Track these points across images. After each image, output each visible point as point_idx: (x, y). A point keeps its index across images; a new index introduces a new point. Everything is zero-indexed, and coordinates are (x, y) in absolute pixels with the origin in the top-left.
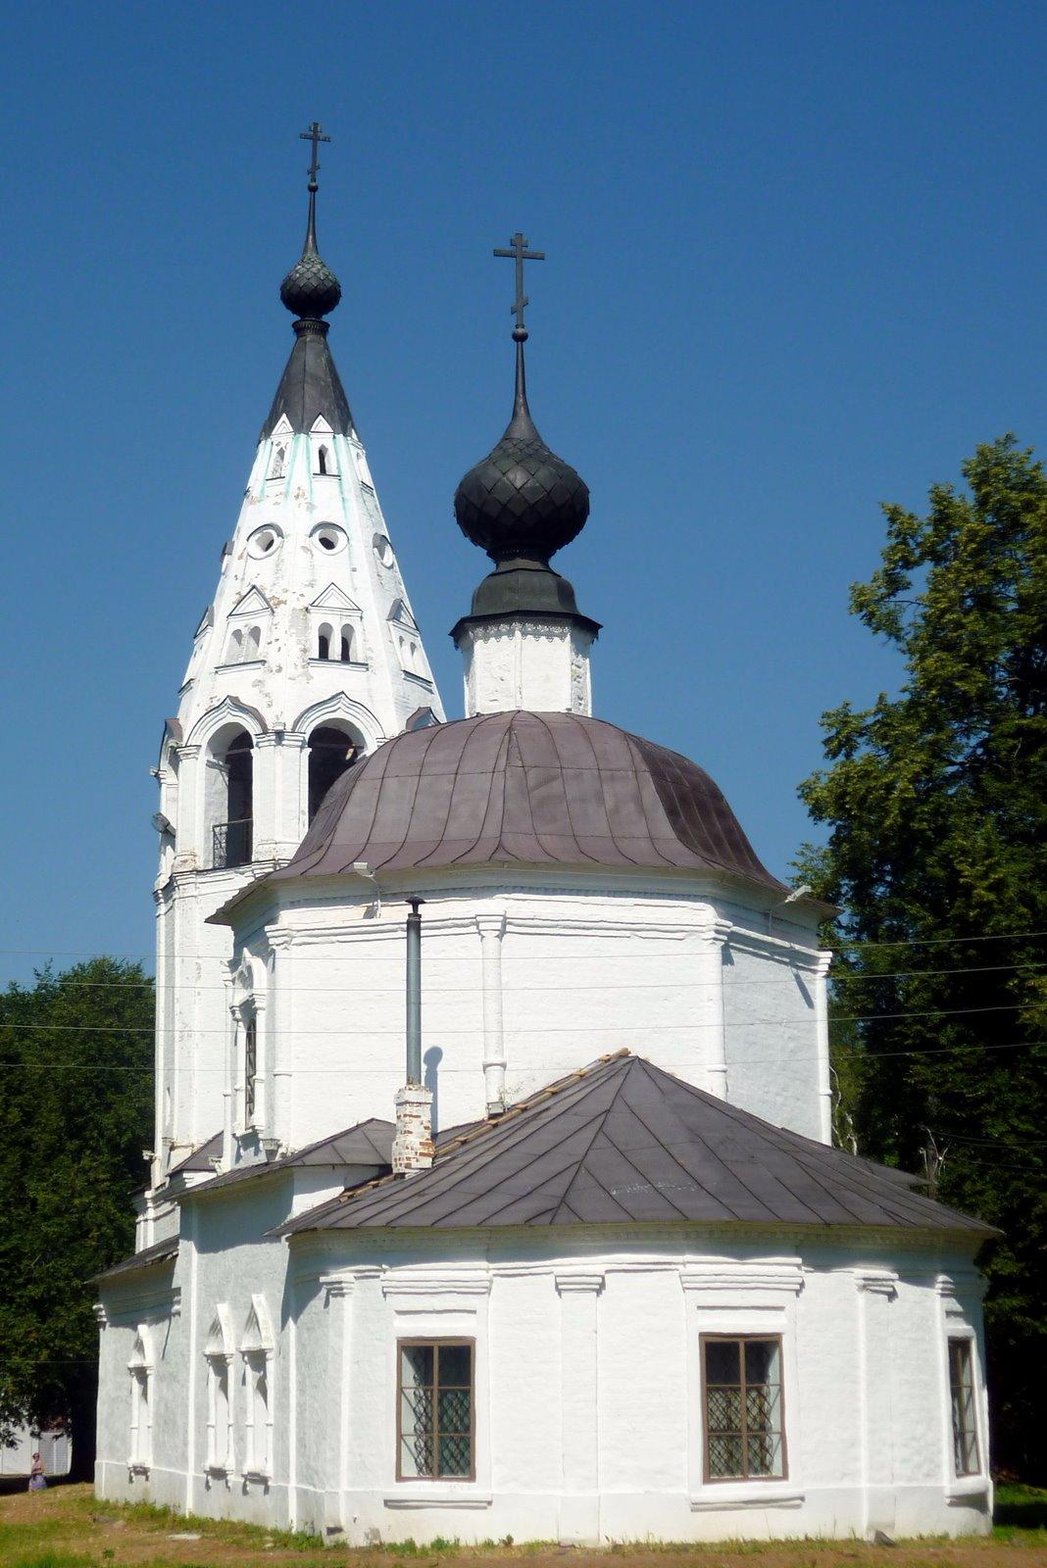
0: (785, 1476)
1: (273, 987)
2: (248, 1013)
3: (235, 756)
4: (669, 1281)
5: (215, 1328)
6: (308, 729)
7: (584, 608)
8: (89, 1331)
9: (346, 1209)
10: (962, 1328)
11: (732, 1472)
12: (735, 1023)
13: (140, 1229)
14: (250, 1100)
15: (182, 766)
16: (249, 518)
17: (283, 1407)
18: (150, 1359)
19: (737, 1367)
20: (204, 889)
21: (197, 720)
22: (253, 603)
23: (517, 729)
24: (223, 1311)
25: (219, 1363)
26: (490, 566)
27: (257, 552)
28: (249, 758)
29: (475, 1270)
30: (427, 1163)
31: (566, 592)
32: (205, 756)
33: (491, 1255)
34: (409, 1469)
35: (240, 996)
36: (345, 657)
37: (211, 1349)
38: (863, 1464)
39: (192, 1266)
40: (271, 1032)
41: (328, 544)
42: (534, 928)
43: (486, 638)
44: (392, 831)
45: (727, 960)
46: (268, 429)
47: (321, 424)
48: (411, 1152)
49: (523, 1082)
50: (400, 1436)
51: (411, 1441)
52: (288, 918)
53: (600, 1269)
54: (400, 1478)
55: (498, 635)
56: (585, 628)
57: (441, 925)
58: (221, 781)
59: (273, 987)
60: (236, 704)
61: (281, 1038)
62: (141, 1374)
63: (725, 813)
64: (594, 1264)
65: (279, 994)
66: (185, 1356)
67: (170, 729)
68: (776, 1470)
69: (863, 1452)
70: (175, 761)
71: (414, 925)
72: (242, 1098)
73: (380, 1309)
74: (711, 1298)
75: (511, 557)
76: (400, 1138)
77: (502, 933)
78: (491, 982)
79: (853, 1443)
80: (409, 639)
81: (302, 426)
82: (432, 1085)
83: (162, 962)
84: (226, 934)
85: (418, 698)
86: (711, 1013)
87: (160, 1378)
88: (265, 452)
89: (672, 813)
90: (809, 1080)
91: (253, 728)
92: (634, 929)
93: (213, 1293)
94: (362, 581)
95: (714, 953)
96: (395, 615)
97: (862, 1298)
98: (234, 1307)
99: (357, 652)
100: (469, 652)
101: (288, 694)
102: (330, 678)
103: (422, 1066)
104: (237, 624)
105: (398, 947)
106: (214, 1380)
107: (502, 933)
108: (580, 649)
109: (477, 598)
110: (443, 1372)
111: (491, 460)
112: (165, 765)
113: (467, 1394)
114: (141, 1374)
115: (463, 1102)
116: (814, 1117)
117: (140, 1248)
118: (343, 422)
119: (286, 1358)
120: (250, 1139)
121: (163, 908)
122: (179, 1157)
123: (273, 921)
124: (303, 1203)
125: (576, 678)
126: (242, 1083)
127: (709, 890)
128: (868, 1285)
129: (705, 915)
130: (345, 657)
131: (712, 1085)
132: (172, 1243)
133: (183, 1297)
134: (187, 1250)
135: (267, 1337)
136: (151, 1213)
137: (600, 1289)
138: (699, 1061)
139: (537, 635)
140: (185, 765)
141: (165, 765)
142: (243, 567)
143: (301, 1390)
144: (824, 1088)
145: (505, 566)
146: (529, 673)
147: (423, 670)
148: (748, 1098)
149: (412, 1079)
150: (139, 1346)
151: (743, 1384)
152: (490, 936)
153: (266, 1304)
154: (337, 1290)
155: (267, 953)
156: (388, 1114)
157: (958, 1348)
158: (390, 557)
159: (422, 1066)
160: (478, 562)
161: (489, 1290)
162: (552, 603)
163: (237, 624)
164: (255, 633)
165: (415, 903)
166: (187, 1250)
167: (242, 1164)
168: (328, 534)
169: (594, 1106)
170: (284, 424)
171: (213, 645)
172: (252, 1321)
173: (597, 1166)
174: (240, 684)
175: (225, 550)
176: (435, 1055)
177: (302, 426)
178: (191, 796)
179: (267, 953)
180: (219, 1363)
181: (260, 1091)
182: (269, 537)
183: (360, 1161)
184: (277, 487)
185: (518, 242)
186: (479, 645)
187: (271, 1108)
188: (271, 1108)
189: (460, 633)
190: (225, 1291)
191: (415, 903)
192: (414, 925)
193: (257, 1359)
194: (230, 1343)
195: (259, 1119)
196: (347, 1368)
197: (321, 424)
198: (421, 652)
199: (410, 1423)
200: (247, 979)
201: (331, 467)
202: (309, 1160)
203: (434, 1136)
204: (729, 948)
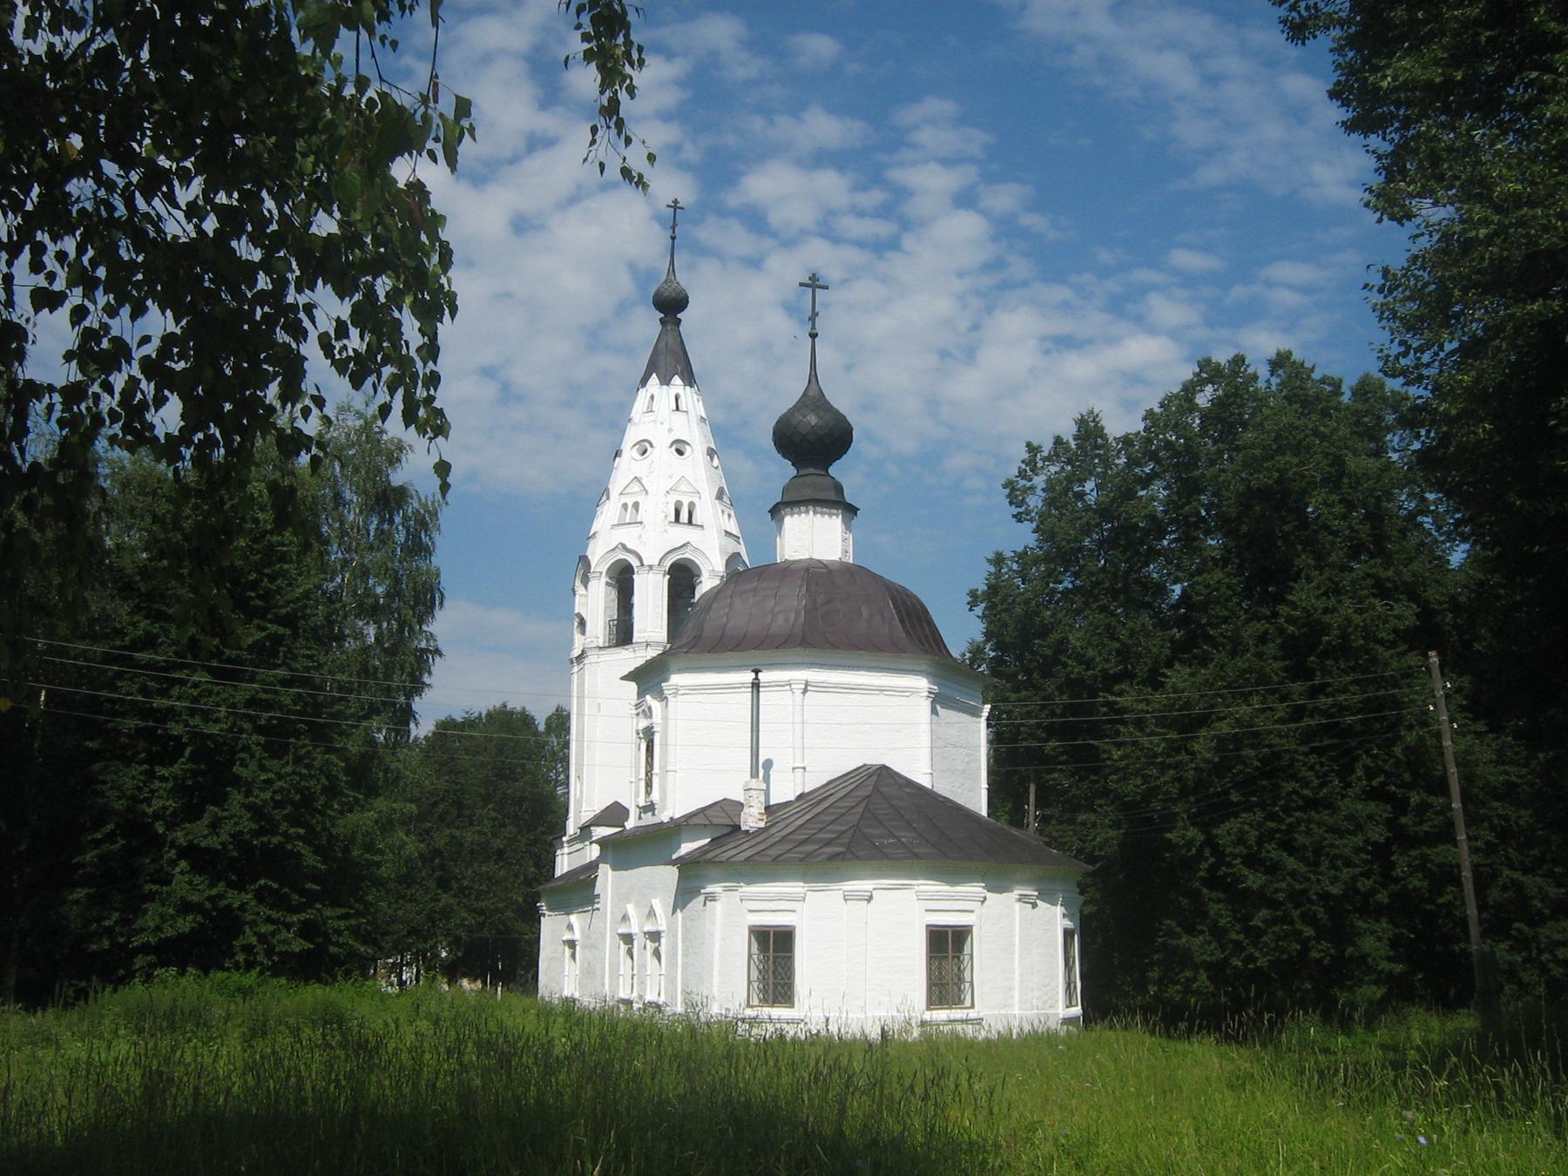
0: (972, 1006)
1: (665, 718)
2: (648, 734)
3: (623, 578)
4: (909, 895)
5: (625, 918)
6: (668, 564)
7: (848, 499)
8: (534, 919)
9: (715, 848)
10: (1069, 924)
11: (941, 1003)
12: (938, 746)
13: (558, 860)
14: (649, 785)
15: (590, 585)
16: (632, 435)
17: (672, 964)
18: (577, 936)
19: (946, 945)
20: (602, 658)
21: (600, 554)
22: (636, 487)
23: (814, 575)
24: (631, 909)
25: (628, 939)
26: (791, 470)
27: (638, 457)
28: (632, 581)
29: (795, 887)
30: (762, 825)
31: (839, 489)
32: (604, 579)
33: (806, 878)
34: (756, 1002)
35: (643, 723)
36: (690, 522)
37: (622, 930)
38: (1016, 1000)
39: (607, 878)
40: (664, 745)
41: (680, 452)
42: (825, 688)
43: (792, 515)
44: (716, 624)
45: (934, 712)
46: (644, 382)
47: (677, 380)
48: (752, 819)
49: (813, 782)
50: (749, 982)
51: (755, 985)
52: (676, 679)
53: (870, 888)
54: (749, 1006)
55: (799, 513)
56: (850, 510)
57: (770, 685)
58: (614, 594)
59: (665, 718)
60: (624, 547)
61: (671, 749)
62: (572, 944)
63: (930, 623)
64: (865, 885)
65: (671, 723)
66: (603, 935)
67: (584, 561)
68: (968, 1003)
69: (1016, 994)
70: (585, 581)
71: (756, 685)
72: (643, 784)
73: (735, 909)
74: (932, 905)
75: (806, 466)
76: (746, 810)
77: (805, 691)
78: (798, 719)
79: (1011, 988)
80: (727, 511)
81: (666, 381)
82: (767, 779)
83: (575, 701)
84: (632, 687)
85: (732, 547)
86: (925, 739)
87: (584, 947)
88: (643, 395)
89: (902, 621)
90: (977, 779)
91: (634, 562)
92: (881, 690)
93: (621, 898)
94: (698, 476)
95: (926, 705)
96: (720, 495)
97: (1017, 906)
98: (638, 906)
99: (697, 519)
100: (781, 522)
101: (654, 544)
102: (681, 534)
103: (760, 767)
104: (624, 500)
105: (746, 697)
106: (624, 948)
107: (805, 691)
108: (847, 525)
109: (785, 490)
110: (775, 949)
111: (797, 408)
112: (578, 583)
113: (789, 959)
114: (572, 944)
115: (784, 790)
116: (979, 804)
117: (558, 873)
118: (690, 379)
119: (675, 936)
120: (650, 808)
121: (576, 669)
122: (586, 817)
123: (667, 680)
124: (686, 848)
125: (844, 540)
126: (643, 775)
127: (924, 667)
128: (1022, 898)
129: (922, 684)
130: (690, 522)
131: (925, 782)
132: (592, 867)
133: (602, 899)
134: (605, 871)
135: (662, 925)
136: (566, 850)
137: (870, 899)
138: (917, 768)
139: (823, 514)
140: (592, 584)
141: (578, 583)
142: (628, 466)
143: (685, 955)
144: (984, 785)
145: (803, 472)
146: (813, 537)
147: (735, 531)
148: (944, 788)
149: (755, 774)
150: (570, 927)
151: (950, 954)
152: (798, 693)
153: (661, 905)
154: (711, 898)
155: (662, 697)
156: (738, 796)
157: (1068, 934)
158: (716, 462)
159: (760, 767)
160: (788, 469)
161: (804, 899)
162: (832, 496)
163: (624, 500)
164: (636, 505)
165: (757, 672)
166: (605, 871)
167: (642, 823)
168: (680, 446)
169: (863, 793)
170: (654, 379)
171: (608, 514)
172: (651, 913)
173: (867, 825)
174: (629, 537)
175: (618, 454)
176: (769, 764)
177: (666, 381)
178: (595, 602)
179: (662, 697)
180: (628, 939)
181: (656, 780)
182: (644, 448)
183: (720, 822)
184: (649, 417)
185: (814, 278)
186: (788, 520)
187: (663, 791)
188: (663, 791)
189: (776, 512)
190: (635, 896)
191: (757, 672)
192: (756, 685)
193: (655, 936)
194: (634, 927)
195: (655, 796)
196: (717, 943)
197: (677, 380)
198: (733, 519)
199: (755, 974)
200: (648, 713)
201: (682, 406)
202: (691, 822)
203: (768, 808)
204: (939, 701)
